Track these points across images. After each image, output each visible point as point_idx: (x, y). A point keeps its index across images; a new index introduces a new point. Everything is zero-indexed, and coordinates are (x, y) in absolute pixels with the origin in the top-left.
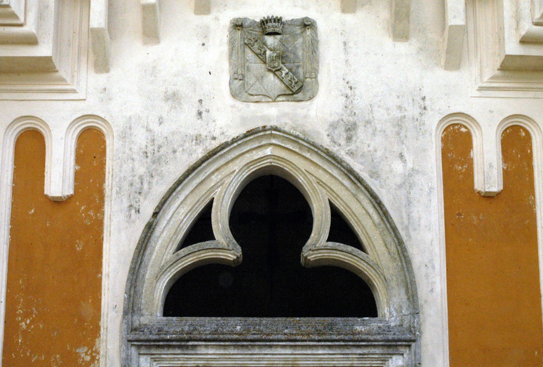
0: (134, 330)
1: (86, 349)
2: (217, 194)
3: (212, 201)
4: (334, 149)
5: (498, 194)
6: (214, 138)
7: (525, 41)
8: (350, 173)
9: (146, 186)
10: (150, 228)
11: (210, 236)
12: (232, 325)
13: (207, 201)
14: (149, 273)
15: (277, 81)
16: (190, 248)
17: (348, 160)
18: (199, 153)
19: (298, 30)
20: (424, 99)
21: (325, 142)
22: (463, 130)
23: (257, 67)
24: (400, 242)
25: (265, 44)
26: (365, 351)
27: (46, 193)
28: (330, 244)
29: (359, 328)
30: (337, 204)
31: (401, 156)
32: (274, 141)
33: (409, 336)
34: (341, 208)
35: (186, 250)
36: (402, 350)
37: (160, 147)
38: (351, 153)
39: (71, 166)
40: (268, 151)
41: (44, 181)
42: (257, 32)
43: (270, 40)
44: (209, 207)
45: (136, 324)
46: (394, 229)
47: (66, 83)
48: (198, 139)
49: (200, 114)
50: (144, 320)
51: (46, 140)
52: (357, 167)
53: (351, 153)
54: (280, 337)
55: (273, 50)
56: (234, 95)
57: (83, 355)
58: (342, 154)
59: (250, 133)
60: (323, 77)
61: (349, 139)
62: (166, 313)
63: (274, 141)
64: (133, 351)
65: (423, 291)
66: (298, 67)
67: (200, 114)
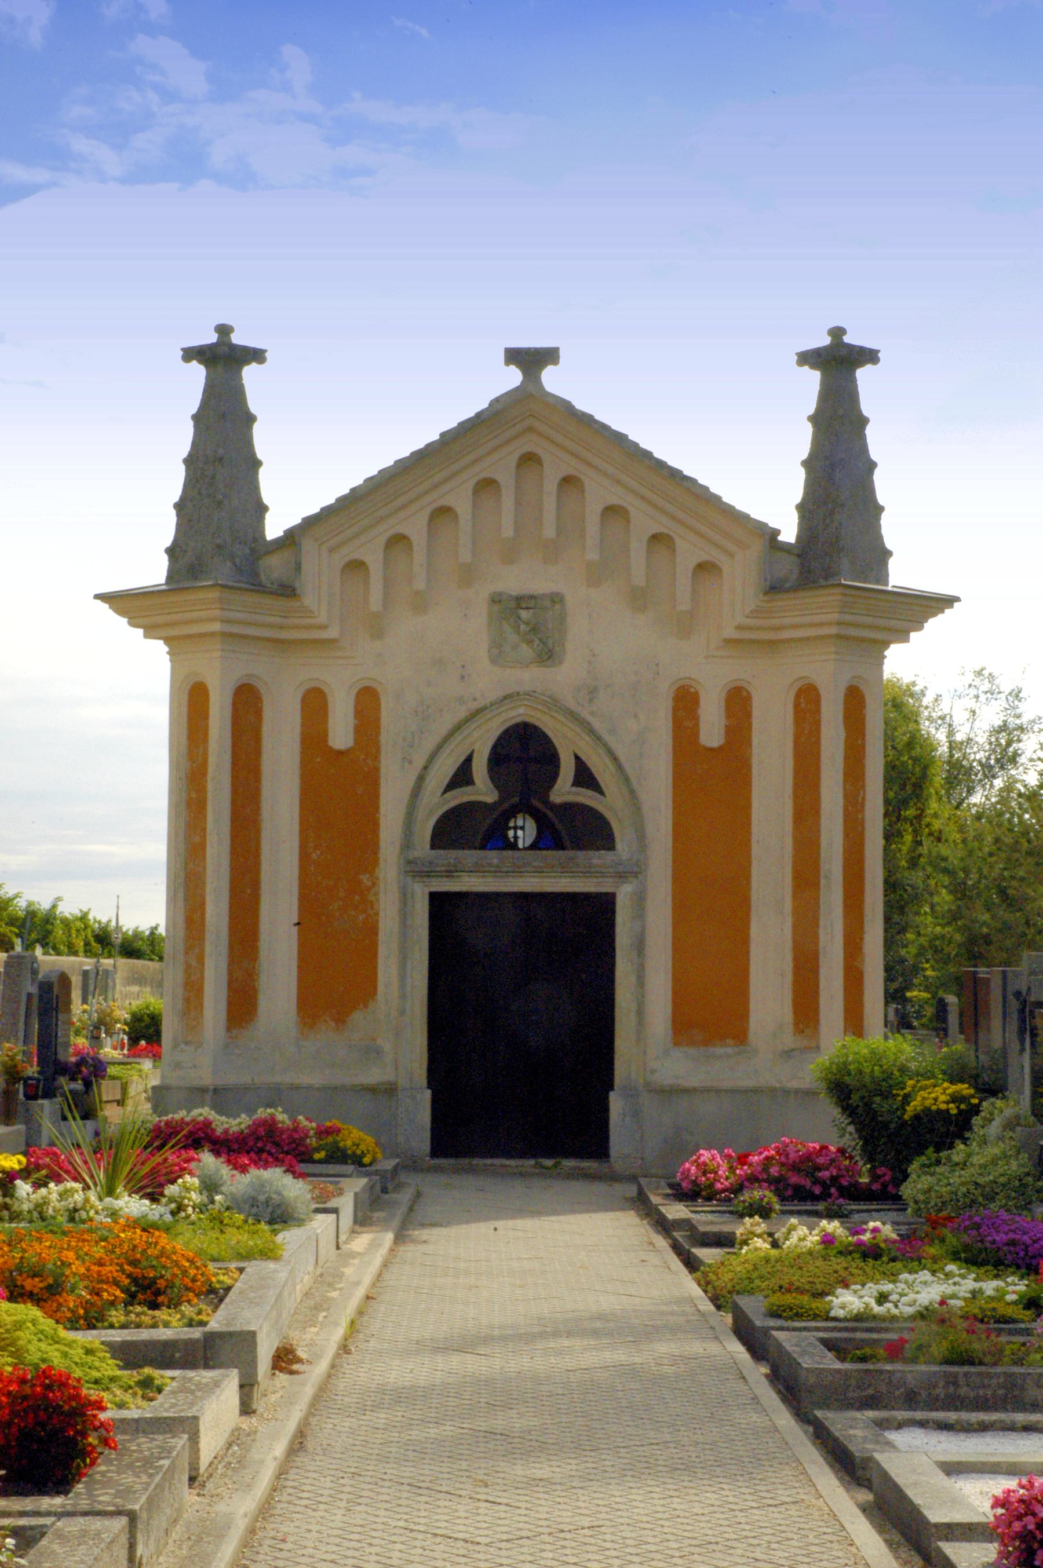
0: (409, 862)
1: (367, 876)
2: (477, 747)
3: (473, 751)
4: (578, 709)
5: (721, 748)
6: (475, 700)
7: (739, 628)
8: (591, 731)
9: (416, 740)
10: (421, 779)
11: (470, 782)
12: (949, 819)
13: (469, 752)
14: (421, 813)
15: (530, 650)
16: (454, 792)
17: (590, 718)
18: (462, 713)
19: (548, 603)
20: (657, 665)
21: (570, 702)
22: (692, 690)
23: (513, 637)
24: (632, 792)
25: (519, 618)
26: (601, 880)
27: (331, 743)
28: (574, 789)
29: (595, 861)
30: (580, 754)
31: (636, 716)
32: (526, 703)
33: (636, 869)
34: (584, 758)
35: (448, 795)
36: (630, 879)
37: (428, 707)
38: (592, 714)
39: (351, 721)
40: (521, 710)
41: (303, 725)
42: (513, 604)
43: (524, 614)
44: (469, 760)
45: (411, 858)
46: (627, 780)
47: (308, 621)
48: (461, 700)
49: (463, 677)
50: (416, 854)
51: (330, 699)
52: (596, 724)
53: (592, 714)
54: (529, 869)
55: (527, 623)
56: (493, 661)
57: (365, 881)
58: (585, 714)
59: (505, 698)
60: (569, 646)
61: (591, 700)
62: (433, 846)
63: (526, 703)
64: (409, 879)
65: (650, 829)
66: (547, 638)
67: (463, 677)
